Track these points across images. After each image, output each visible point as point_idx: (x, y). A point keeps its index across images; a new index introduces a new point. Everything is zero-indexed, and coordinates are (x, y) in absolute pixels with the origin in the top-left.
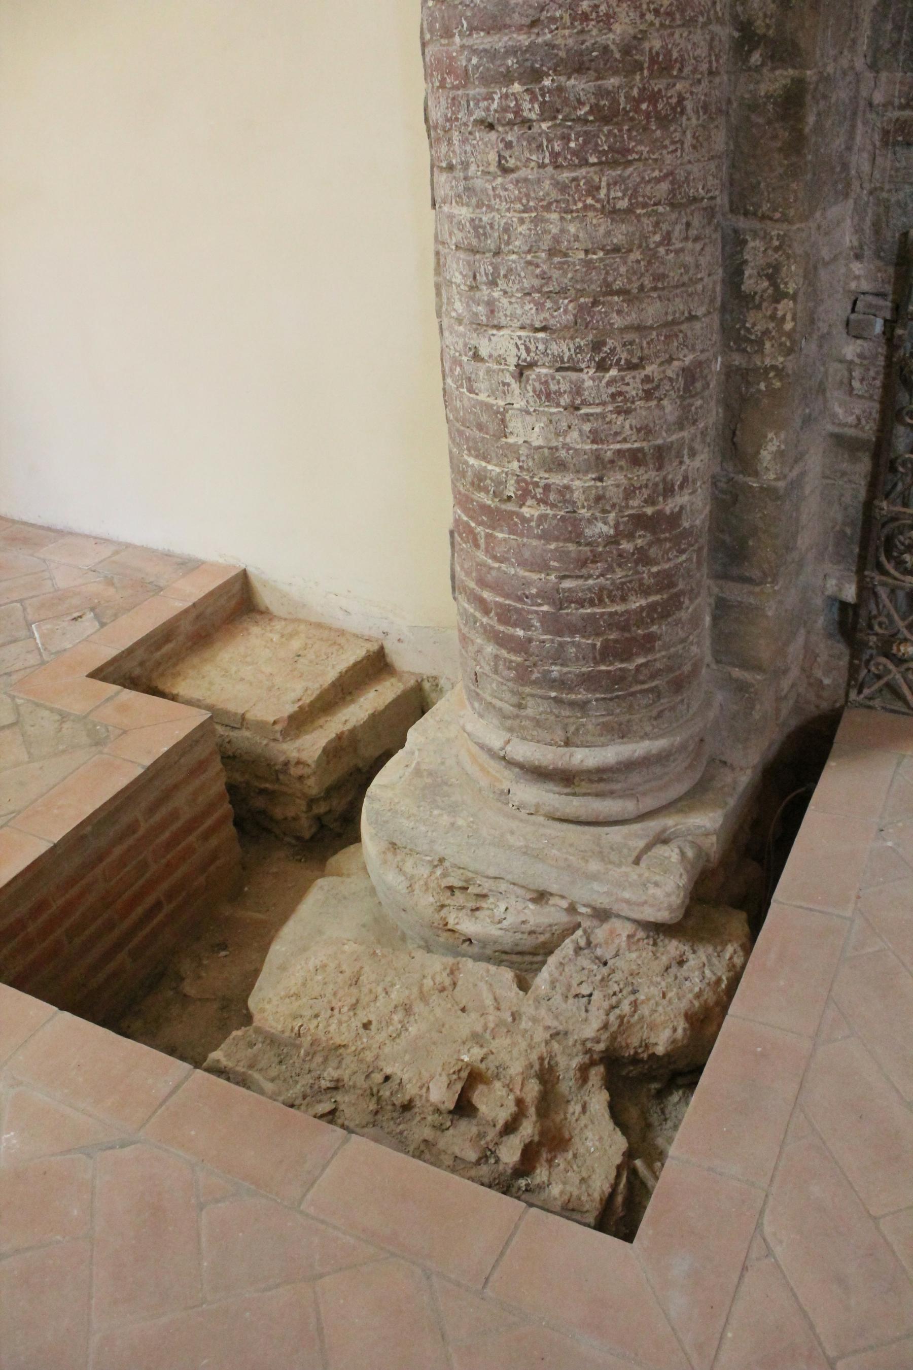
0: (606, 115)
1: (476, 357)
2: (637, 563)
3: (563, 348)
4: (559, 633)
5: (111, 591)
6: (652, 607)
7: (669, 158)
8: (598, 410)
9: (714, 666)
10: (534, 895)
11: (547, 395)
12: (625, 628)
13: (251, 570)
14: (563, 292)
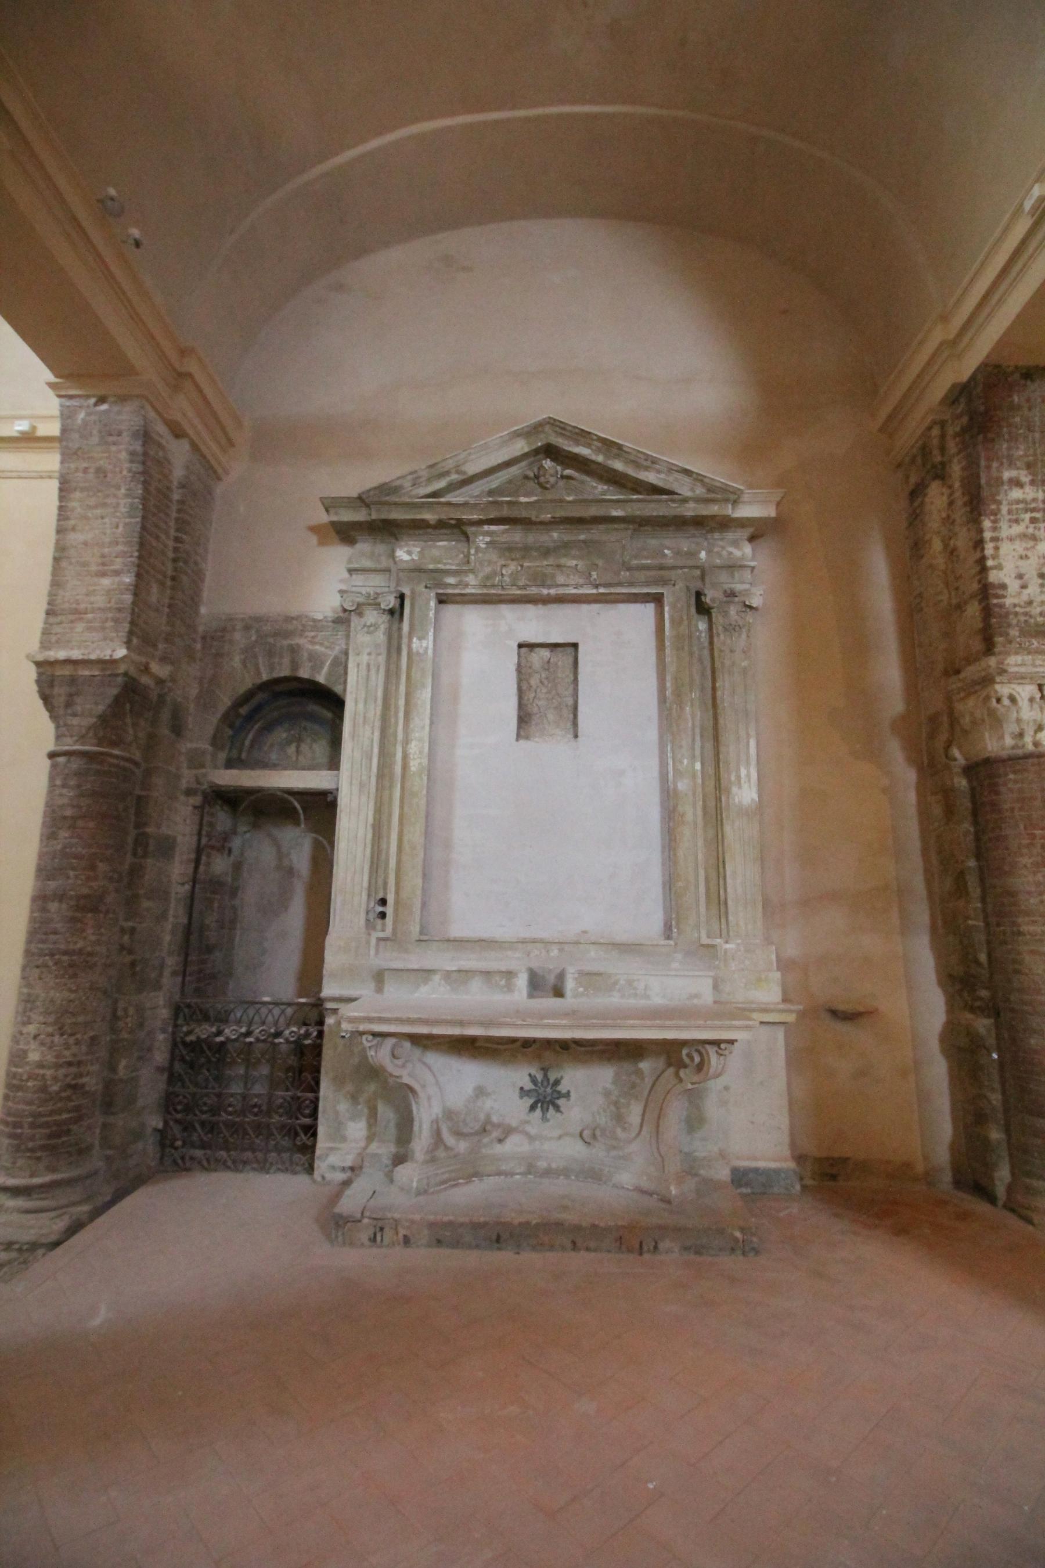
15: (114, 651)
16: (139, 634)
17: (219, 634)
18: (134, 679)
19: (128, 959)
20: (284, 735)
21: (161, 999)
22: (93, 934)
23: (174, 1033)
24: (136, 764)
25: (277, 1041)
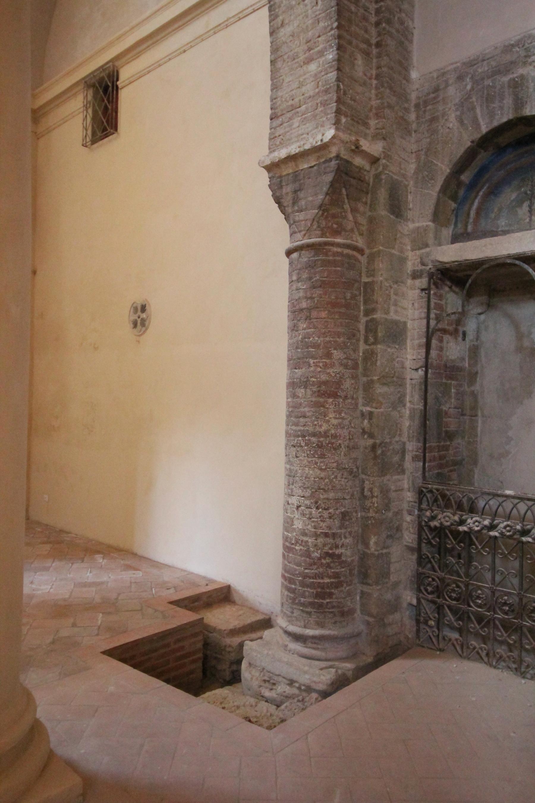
0: (320, 446)
1: (288, 504)
2: (327, 567)
3: (308, 502)
4: (303, 587)
5: (182, 584)
6: (332, 583)
7: (336, 458)
8: (316, 520)
9: (360, 615)
10: (288, 682)
11: (303, 515)
12: (323, 588)
13: (232, 585)
14: (308, 488)
15: (323, 135)
16: (346, 109)
17: (432, 95)
18: (347, 162)
19: (370, 442)
20: (514, 196)
21: (406, 482)
22: (335, 418)
23: (419, 517)
24: (361, 251)
25: (524, 539)
